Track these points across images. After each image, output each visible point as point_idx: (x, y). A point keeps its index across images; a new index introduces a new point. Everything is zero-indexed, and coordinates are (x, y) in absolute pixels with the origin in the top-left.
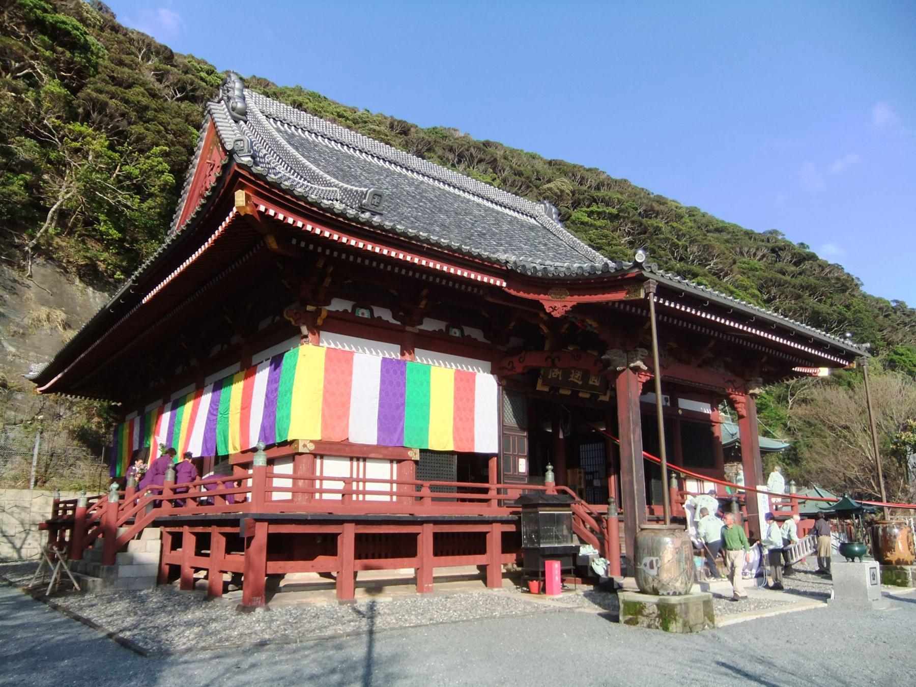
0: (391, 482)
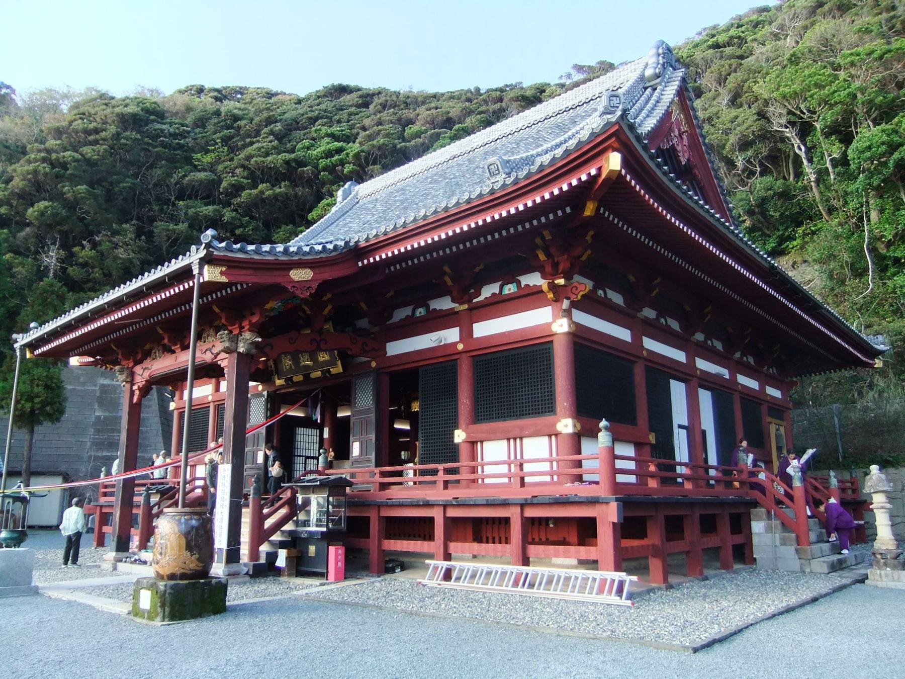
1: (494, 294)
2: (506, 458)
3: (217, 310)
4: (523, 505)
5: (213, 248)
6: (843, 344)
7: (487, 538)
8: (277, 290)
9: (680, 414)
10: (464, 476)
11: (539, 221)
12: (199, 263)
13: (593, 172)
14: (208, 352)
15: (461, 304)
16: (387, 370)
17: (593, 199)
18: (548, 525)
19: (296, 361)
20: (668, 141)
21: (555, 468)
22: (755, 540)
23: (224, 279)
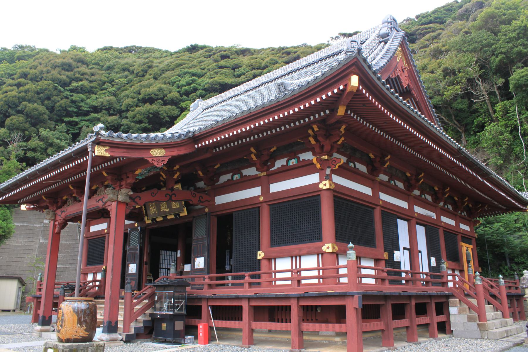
0: (318, 269)
1: (283, 166)
2: (290, 268)
3: (105, 175)
4: (299, 298)
5: (101, 135)
6: (507, 197)
7: (278, 319)
8: (142, 162)
9: (404, 240)
10: (264, 278)
11: (309, 119)
12: (92, 145)
13: (341, 87)
14: (100, 201)
15: (262, 172)
16: (215, 214)
17: (344, 105)
18: (316, 311)
19: (158, 208)
20: (395, 73)
21: (321, 274)
22: (452, 319)
23: (108, 155)
